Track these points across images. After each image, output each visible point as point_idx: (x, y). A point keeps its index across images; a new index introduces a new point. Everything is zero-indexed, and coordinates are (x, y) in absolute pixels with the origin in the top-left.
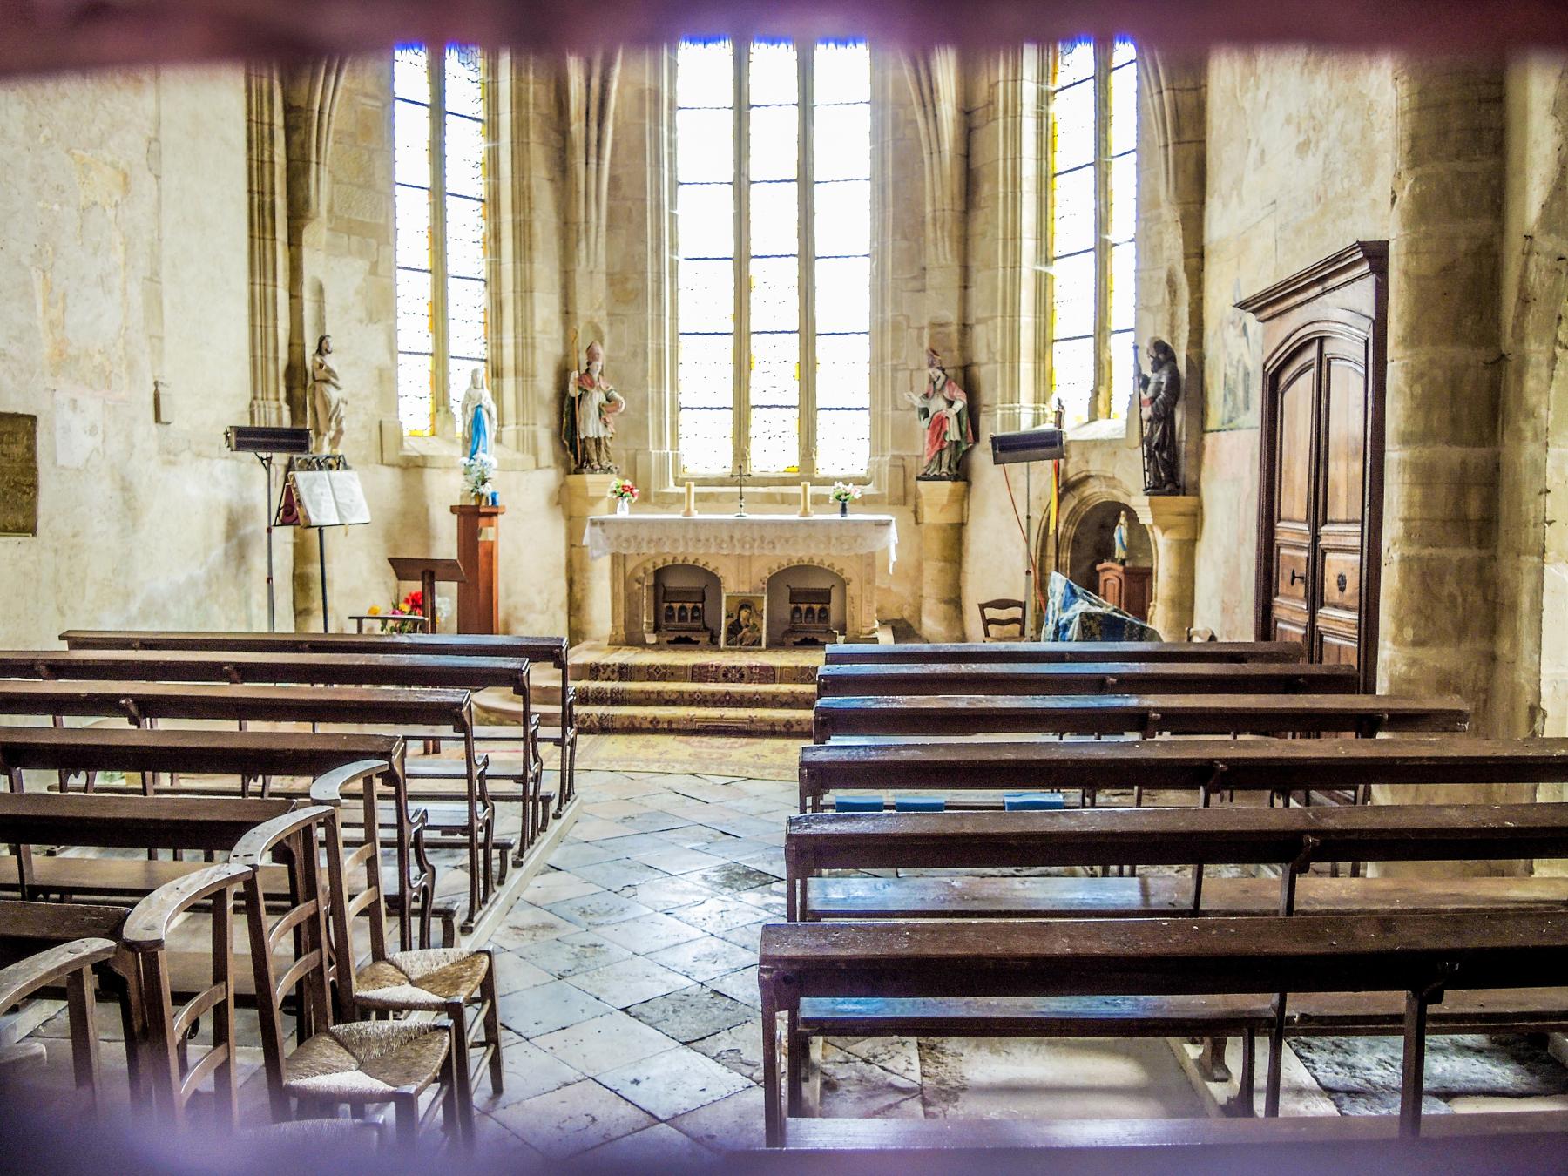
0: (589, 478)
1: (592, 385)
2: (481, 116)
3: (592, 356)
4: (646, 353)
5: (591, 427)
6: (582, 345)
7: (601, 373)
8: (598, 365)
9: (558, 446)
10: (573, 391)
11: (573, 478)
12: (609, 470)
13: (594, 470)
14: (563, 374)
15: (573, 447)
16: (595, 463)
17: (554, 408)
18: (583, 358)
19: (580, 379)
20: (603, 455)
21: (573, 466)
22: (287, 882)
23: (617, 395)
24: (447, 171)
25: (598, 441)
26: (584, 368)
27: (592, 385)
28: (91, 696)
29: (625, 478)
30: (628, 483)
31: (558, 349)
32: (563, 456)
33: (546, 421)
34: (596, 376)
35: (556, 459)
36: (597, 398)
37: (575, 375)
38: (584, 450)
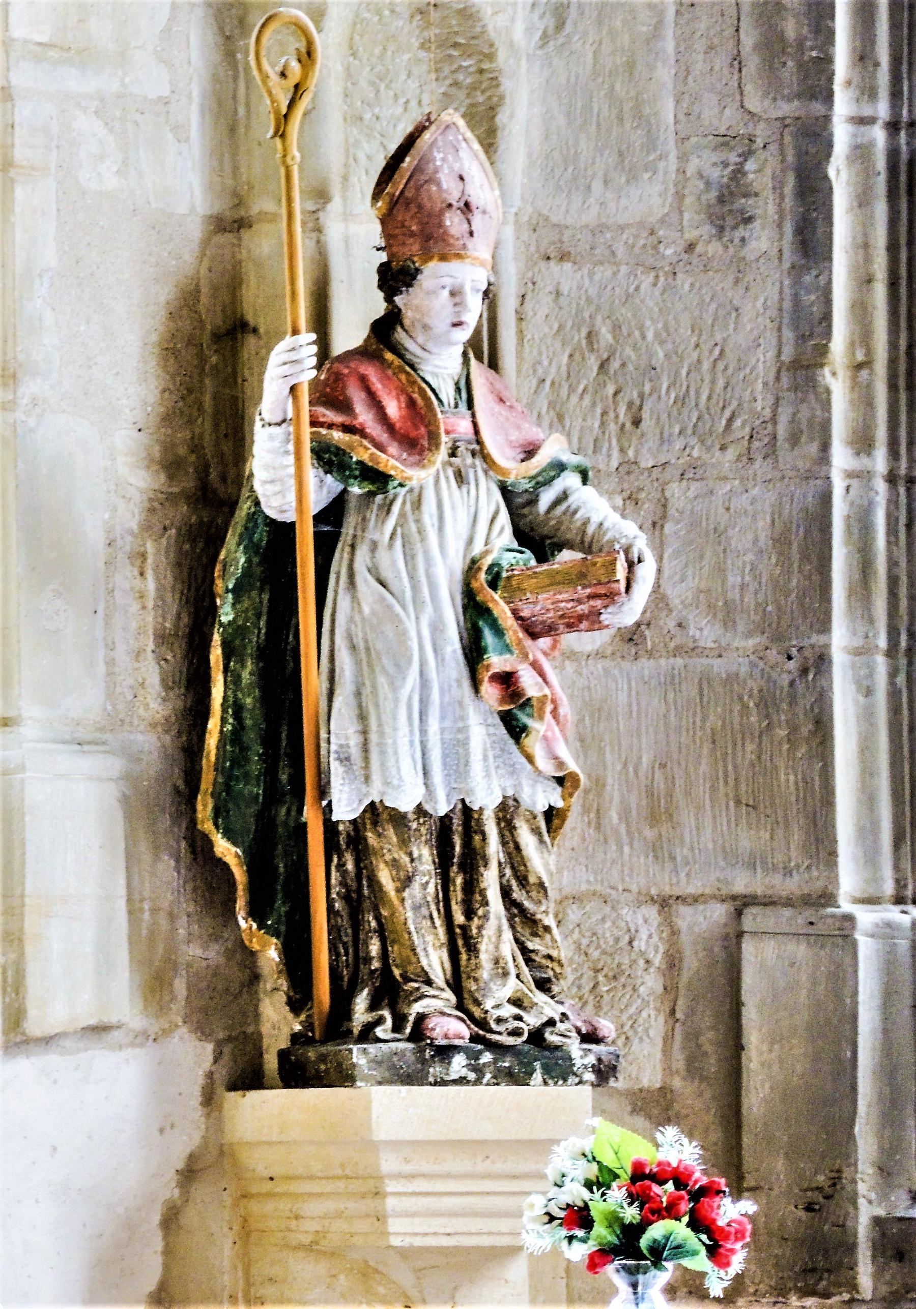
0: (384, 1110)
1: (417, 432)
2: (399, 329)
3: (413, 224)
4: (812, 190)
5: (399, 737)
6: (346, 149)
7: (484, 349)
8: (446, 300)
9: (167, 875)
10: (280, 478)
11: (269, 1114)
12: (533, 1056)
13: (425, 1060)
14: (211, 350)
15: (278, 891)
16: (436, 1007)
17: (140, 603)
18: (356, 238)
19: (330, 393)
20: (496, 936)
21: (277, 1023)
22: (292, 497)
23: (595, 507)
24: (377, 278)
25: (457, 841)
26: (355, 312)
27: (417, 432)
28: (831, 33)
29: (655, 1108)
30: (677, 1149)
31: (184, 187)
32: (198, 952)
33: (87, 701)
34: (442, 366)
35: (155, 984)
36: (450, 522)
37: (285, 369)
38: (360, 900)
